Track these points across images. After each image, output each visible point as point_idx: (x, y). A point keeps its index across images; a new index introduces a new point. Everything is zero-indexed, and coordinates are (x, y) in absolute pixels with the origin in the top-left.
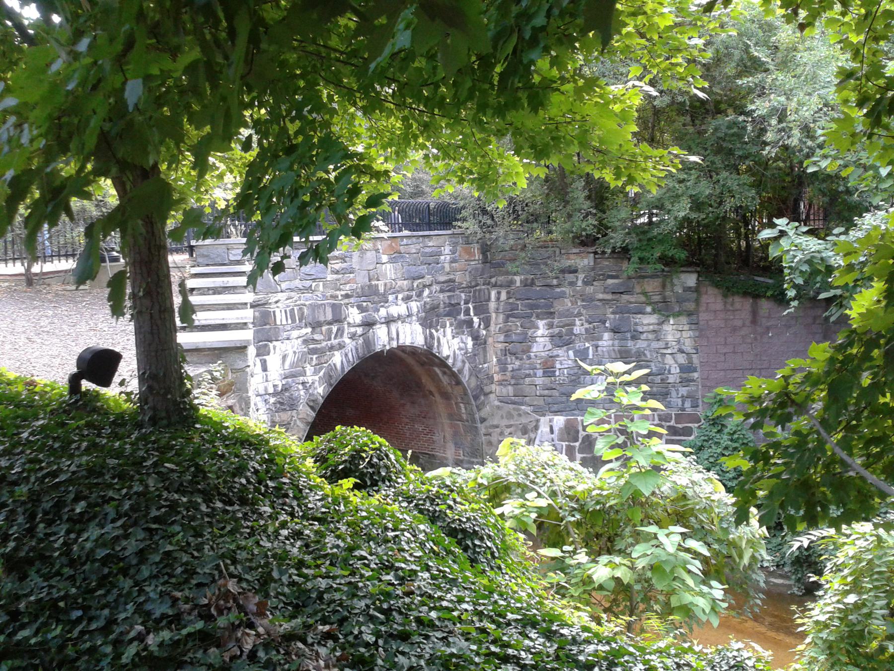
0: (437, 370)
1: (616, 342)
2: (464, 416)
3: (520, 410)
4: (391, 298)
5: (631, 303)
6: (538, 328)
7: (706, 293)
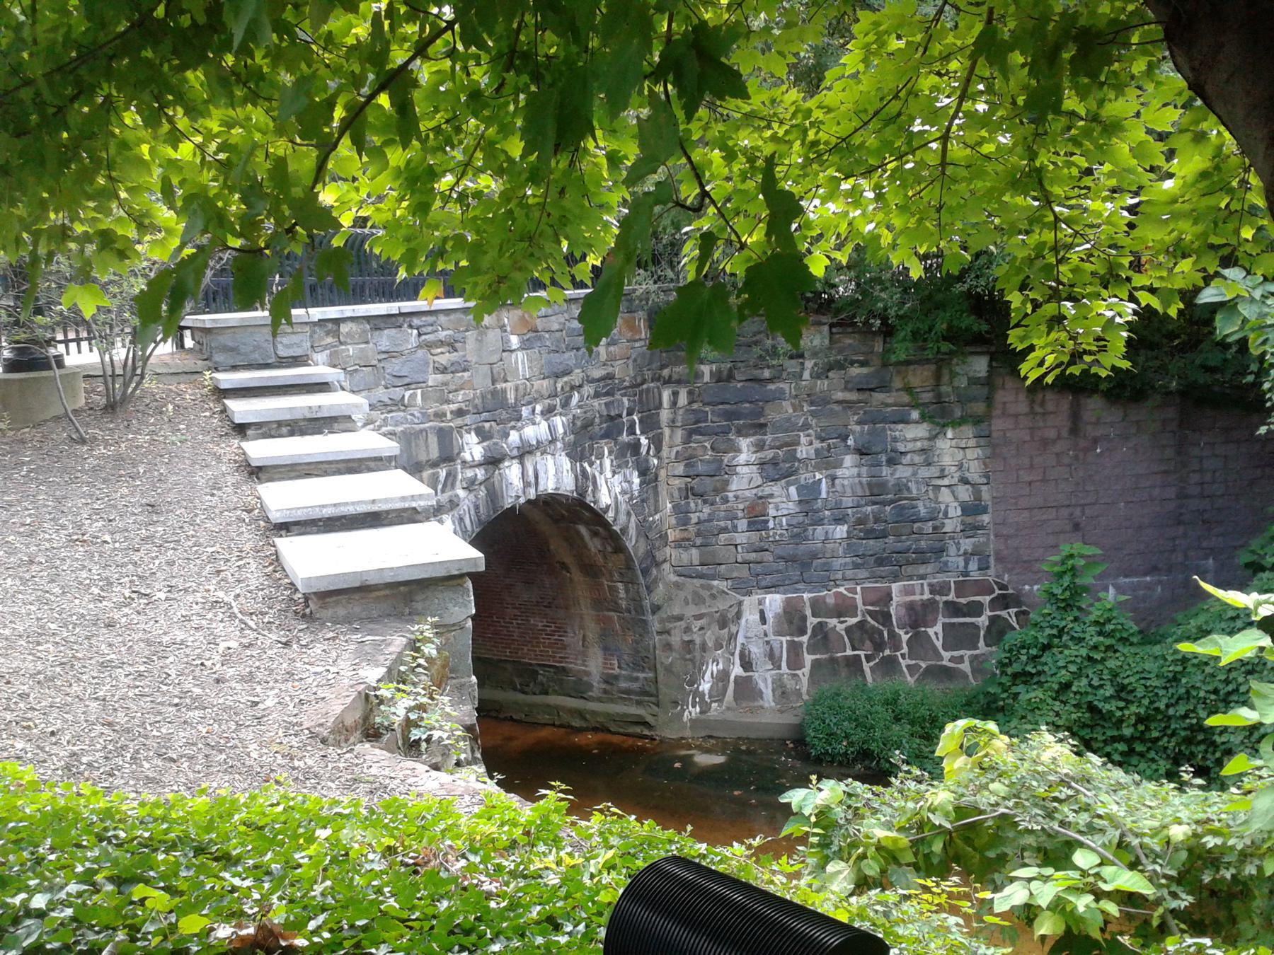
0: (583, 530)
1: (864, 470)
2: (624, 604)
3: (710, 587)
4: (525, 411)
5: (887, 405)
6: (739, 451)
7: (1003, 388)
